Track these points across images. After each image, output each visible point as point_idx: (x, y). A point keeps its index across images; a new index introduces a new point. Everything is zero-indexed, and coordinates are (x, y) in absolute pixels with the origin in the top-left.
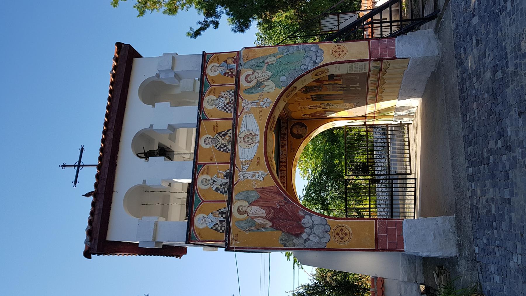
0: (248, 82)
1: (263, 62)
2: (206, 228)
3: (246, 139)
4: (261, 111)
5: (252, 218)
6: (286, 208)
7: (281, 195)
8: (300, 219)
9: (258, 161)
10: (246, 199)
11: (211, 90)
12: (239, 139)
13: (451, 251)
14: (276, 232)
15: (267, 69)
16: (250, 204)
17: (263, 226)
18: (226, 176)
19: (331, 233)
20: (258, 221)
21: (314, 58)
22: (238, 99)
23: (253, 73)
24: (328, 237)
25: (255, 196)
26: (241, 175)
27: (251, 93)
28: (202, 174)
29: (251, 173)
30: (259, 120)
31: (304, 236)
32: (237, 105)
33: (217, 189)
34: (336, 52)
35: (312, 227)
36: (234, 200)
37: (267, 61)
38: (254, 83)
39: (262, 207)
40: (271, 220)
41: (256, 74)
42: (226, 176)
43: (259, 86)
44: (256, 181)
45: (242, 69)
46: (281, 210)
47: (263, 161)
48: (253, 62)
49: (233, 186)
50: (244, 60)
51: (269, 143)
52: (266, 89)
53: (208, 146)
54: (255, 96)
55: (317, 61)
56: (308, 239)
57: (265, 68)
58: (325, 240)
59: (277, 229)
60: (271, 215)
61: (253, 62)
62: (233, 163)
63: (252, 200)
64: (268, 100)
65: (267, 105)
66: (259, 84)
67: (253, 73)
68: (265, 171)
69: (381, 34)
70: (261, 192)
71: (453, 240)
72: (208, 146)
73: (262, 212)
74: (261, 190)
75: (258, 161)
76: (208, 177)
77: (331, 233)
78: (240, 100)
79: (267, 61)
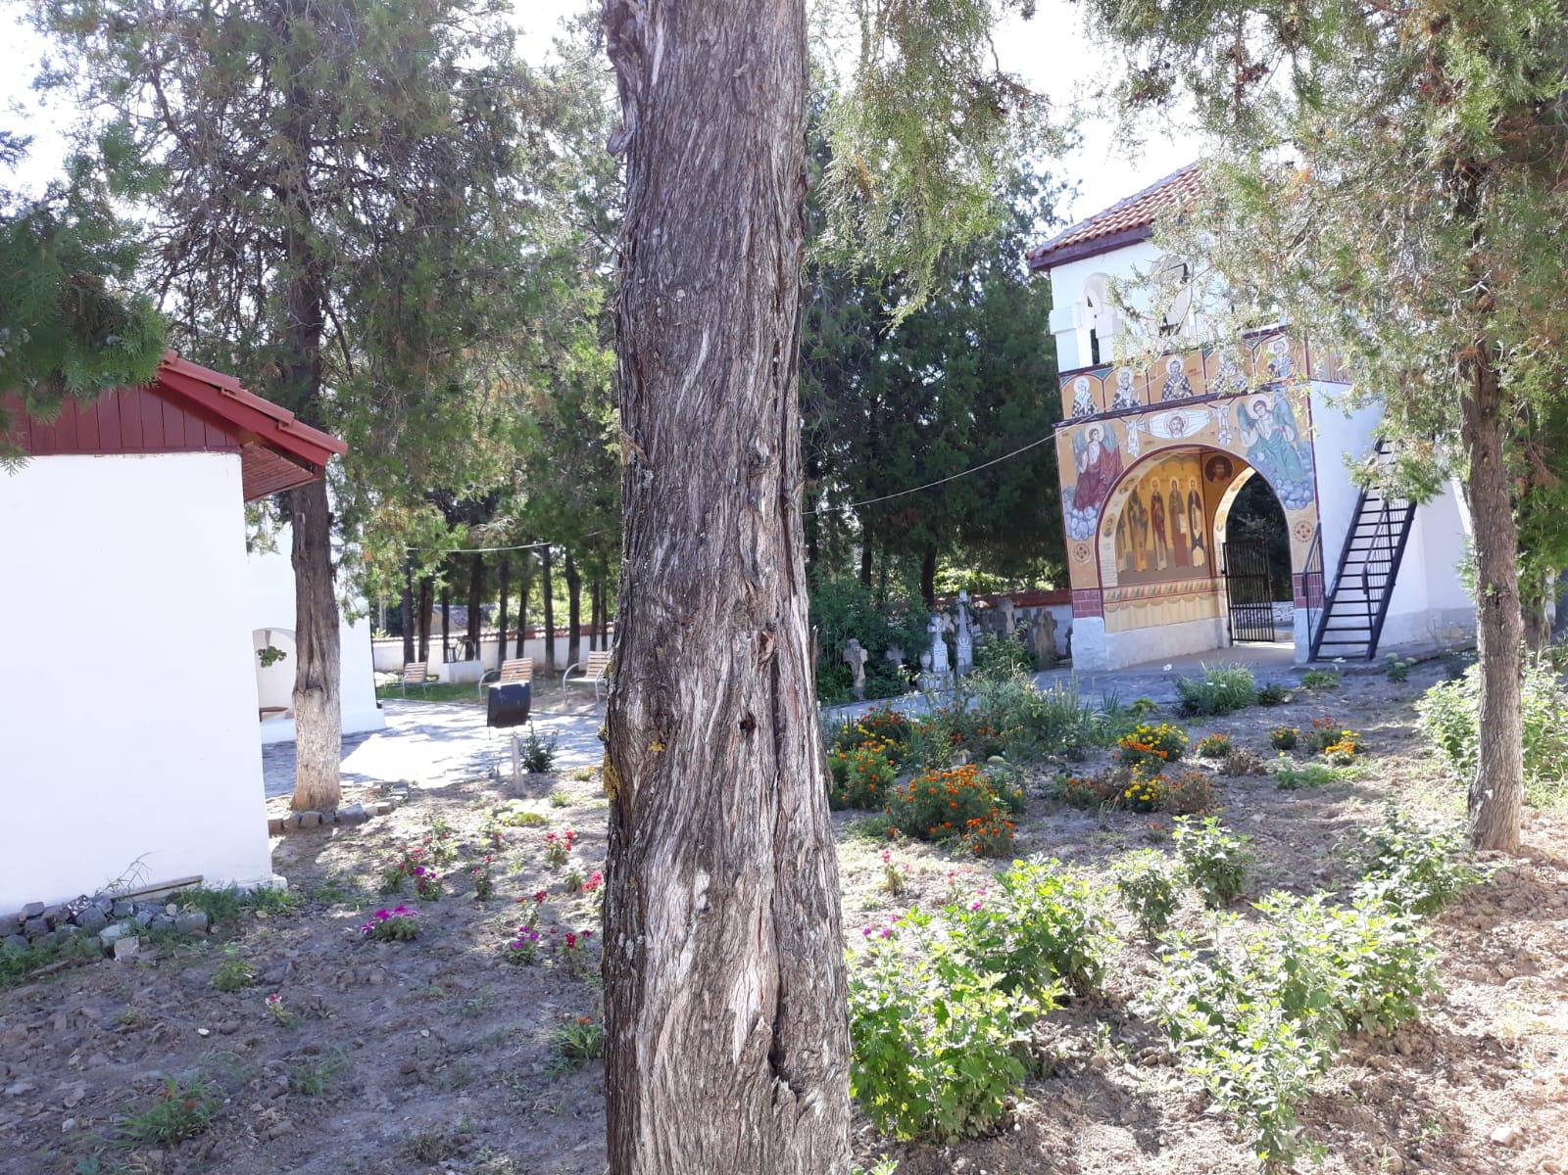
2: (1075, 394)
5: (1087, 449)
6: (1101, 487)
8: (1092, 504)
9: (1149, 443)
10: (1106, 437)
12: (1175, 412)
14: (1076, 479)
16: (1101, 443)
17: (1080, 463)
18: (1134, 404)
20: (1085, 457)
25: (1110, 449)
26: (1133, 425)
30: (1201, 433)
31: (1075, 512)
33: (1117, 396)
35: (1085, 520)
38: (1253, 415)
40: (1087, 472)
42: (1134, 404)
45: (1273, 393)
46: (1099, 481)
48: (1284, 408)
56: (1073, 516)
60: (1092, 470)
61: (1284, 408)
62: (1144, 411)
63: (1106, 444)
66: (1251, 423)
71: (1088, 667)
73: (1094, 460)
74: (1117, 453)
75: (1149, 443)
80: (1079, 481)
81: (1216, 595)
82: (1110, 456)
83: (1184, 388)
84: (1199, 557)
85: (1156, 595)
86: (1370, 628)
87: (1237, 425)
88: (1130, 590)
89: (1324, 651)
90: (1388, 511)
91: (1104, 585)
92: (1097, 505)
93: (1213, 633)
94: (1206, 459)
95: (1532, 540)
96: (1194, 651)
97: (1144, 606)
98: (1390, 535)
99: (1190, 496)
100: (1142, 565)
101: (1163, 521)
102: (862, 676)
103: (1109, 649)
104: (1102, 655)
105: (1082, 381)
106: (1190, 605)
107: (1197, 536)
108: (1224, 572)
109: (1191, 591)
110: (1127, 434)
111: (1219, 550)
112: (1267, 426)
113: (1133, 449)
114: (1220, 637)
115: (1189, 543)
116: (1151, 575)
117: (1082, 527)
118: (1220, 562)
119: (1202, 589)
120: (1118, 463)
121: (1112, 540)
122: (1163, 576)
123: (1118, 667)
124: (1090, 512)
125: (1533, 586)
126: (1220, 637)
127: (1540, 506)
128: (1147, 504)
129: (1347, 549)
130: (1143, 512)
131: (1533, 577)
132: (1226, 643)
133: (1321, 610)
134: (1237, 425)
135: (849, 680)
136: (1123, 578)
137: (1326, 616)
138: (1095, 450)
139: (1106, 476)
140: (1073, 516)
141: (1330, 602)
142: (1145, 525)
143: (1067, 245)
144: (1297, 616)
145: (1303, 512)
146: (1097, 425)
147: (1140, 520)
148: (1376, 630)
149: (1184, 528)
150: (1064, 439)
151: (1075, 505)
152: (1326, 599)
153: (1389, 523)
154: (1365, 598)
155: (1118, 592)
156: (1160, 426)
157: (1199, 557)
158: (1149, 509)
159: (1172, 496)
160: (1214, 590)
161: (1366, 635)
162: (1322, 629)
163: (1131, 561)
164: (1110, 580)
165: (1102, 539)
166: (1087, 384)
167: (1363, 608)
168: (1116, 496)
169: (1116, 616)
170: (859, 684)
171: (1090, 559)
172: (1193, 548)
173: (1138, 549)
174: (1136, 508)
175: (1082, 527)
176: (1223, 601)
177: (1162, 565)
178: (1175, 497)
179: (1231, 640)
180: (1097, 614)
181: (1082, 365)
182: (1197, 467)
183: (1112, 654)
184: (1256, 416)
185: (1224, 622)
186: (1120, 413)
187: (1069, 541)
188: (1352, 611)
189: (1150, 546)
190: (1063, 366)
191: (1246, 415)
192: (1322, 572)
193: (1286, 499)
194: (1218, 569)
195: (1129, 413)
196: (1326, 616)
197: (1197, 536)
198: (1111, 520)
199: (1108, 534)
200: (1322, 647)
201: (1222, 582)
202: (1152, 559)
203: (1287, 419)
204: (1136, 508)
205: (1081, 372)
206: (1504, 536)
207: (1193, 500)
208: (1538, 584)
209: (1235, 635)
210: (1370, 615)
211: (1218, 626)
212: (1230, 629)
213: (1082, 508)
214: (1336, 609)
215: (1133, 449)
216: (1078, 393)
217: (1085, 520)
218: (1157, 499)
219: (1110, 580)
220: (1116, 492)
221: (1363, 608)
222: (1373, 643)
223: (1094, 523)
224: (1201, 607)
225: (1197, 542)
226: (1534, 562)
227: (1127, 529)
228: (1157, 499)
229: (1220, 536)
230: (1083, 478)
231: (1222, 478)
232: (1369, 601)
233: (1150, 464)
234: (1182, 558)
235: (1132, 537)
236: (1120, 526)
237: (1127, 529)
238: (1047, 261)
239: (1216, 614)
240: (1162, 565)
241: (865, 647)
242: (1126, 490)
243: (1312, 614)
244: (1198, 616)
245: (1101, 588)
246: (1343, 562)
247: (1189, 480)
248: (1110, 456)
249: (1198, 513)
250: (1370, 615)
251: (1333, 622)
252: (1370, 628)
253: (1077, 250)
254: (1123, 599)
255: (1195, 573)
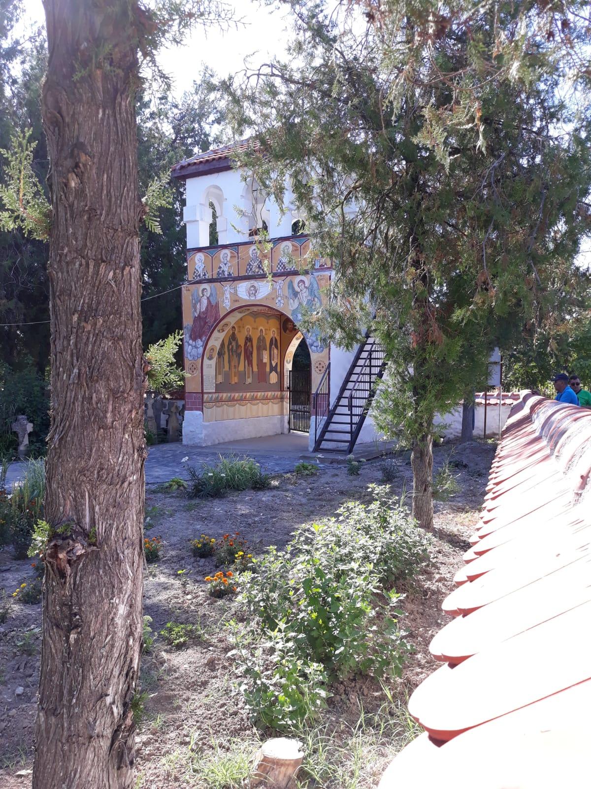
0: (298, 283)
1: (315, 296)
2: (195, 264)
3: (252, 289)
4: (273, 299)
5: (200, 301)
6: (207, 327)
7: (215, 322)
8: (200, 338)
9: (236, 301)
10: (211, 294)
11: (296, 247)
12: (253, 282)
13: (185, 442)
14: (192, 320)
15: (308, 301)
16: (208, 298)
17: (195, 311)
18: (229, 274)
19: (193, 361)
20: (198, 306)
21: (315, 344)
22: (284, 276)
23: (306, 287)
24: (191, 359)
25: (213, 303)
26: (227, 288)
27: (289, 288)
28: (231, 253)
29: (228, 296)
30: (266, 298)
31: (191, 342)
32: (279, 276)
33: (220, 268)
34: (320, 364)
35: (196, 347)
36: (210, 284)
37: (316, 299)
38: (297, 289)
39: (207, 308)
40: (199, 316)
41: (305, 289)
42: (229, 274)
43: (294, 294)
44: (223, 301)
45: (310, 276)
46: (206, 323)
47: (237, 305)
48: (315, 286)
49: (220, 282)
50: (318, 276)
51: (260, 308)
52: (291, 301)
53: (250, 252)
54: (287, 292)
55: (313, 347)
56: (189, 345)
57: (309, 298)
58: (189, 357)
59: (194, 321)
60: (202, 316)
61: (315, 286)
62: (235, 279)
63: (211, 299)
64: (282, 305)
65: (278, 305)
66: (296, 294)
67: (306, 287)
68: (230, 308)
69: (354, 406)
70: (216, 306)
71: (191, 443)
72: (250, 252)
73: (203, 309)
74: (217, 305)
75: (236, 301)
76: (228, 258)
77: (193, 361)
78: (283, 278)
79: (316, 299)
80: (194, 321)
81: (282, 402)
82: (213, 307)
83: (259, 267)
84: (274, 378)
85: (242, 399)
86: (351, 432)
87: (287, 294)
88: (224, 395)
89: (325, 445)
90: (371, 359)
91: (205, 391)
92: (204, 339)
93: (278, 425)
94: (283, 319)
95: (424, 387)
96: (270, 433)
97: (234, 406)
98: (370, 374)
99: (272, 339)
100: (235, 380)
101: (252, 354)
102: (26, 441)
103: (204, 432)
104: (200, 436)
105: (200, 256)
106: (265, 407)
107: (274, 365)
108: (289, 388)
109: (267, 399)
110: (223, 294)
111: (286, 374)
112: (305, 296)
113: (227, 304)
114: (282, 427)
115: (268, 369)
116: (241, 387)
117: (194, 352)
118: (287, 382)
119: (274, 398)
120: (217, 312)
121: (213, 362)
122: (249, 388)
123: (209, 444)
124: (200, 343)
125: (421, 424)
126: (282, 427)
127: (433, 356)
128: (242, 342)
129: (347, 381)
130: (238, 346)
131: (422, 418)
132: (286, 431)
133: (326, 418)
134: (287, 294)
135: (15, 444)
136: (219, 388)
137: (328, 422)
138: (205, 302)
139: (211, 320)
140: (189, 345)
141: (332, 414)
142: (239, 356)
143: (195, 163)
144: (316, 422)
145: (321, 354)
146: (205, 286)
147: (236, 352)
148: (355, 434)
149: (266, 359)
150: (188, 293)
151: (191, 337)
152: (329, 411)
153: (370, 366)
154: (349, 413)
155: (215, 396)
156: (243, 289)
157: (274, 378)
158: (243, 345)
159: (259, 339)
160: (282, 398)
161: (348, 437)
162: (325, 430)
163: (227, 376)
164: (209, 387)
165: (206, 361)
166: (203, 258)
167: (347, 419)
168: (216, 334)
169: (211, 411)
170: (22, 448)
171: (197, 373)
172: (271, 372)
173: (233, 370)
174: (234, 343)
175: (194, 352)
176: (287, 405)
177: (249, 381)
178: (261, 340)
179: (290, 429)
180: (197, 409)
181: (202, 245)
182: (278, 323)
183: (206, 435)
184: (299, 290)
185: (286, 418)
186: (220, 279)
187: (186, 360)
188: (342, 422)
189: (241, 368)
190: (189, 246)
191: (293, 289)
192: (329, 394)
193: (312, 345)
194: (285, 386)
195: (225, 280)
196: (328, 422)
197: (274, 365)
198: (212, 349)
199: (210, 358)
200: (323, 442)
201: (287, 394)
202: (242, 376)
203: (316, 294)
204: (234, 343)
205: (200, 250)
206: (102, 390)
207: (273, 342)
208: (425, 424)
209: (292, 427)
210: (351, 424)
211: (282, 421)
212: (289, 423)
213: (194, 339)
214: (336, 418)
215: (227, 304)
216: (198, 264)
217: (196, 347)
218: (249, 339)
219: (209, 387)
220: (216, 331)
221: (347, 419)
222: (353, 442)
223: (201, 350)
224: (273, 408)
225: (273, 369)
226: (423, 404)
227: (226, 357)
228: (249, 339)
229: (289, 366)
230: (197, 319)
231: (291, 331)
232: (351, 415)
233: (238, 316)
234: (262, 377)
235: (229, 362)
236: (220, 354)
237: (226, 357)
238: (184, 172)
239: (282, 414)
240: (249, 381)
241: (31, 422)
242: (223, 331)
243: (319, 420)
244: (270, 414)
245: (202, 393)
246: (343, 389)
247: (272, 331)
248: (213, 307)
249: (276, 351)
250: (351, 424)
251: (332, 427)
252: (351, 432)
253: (202, 168)
254: (218, 401)
255: (271, 388)
